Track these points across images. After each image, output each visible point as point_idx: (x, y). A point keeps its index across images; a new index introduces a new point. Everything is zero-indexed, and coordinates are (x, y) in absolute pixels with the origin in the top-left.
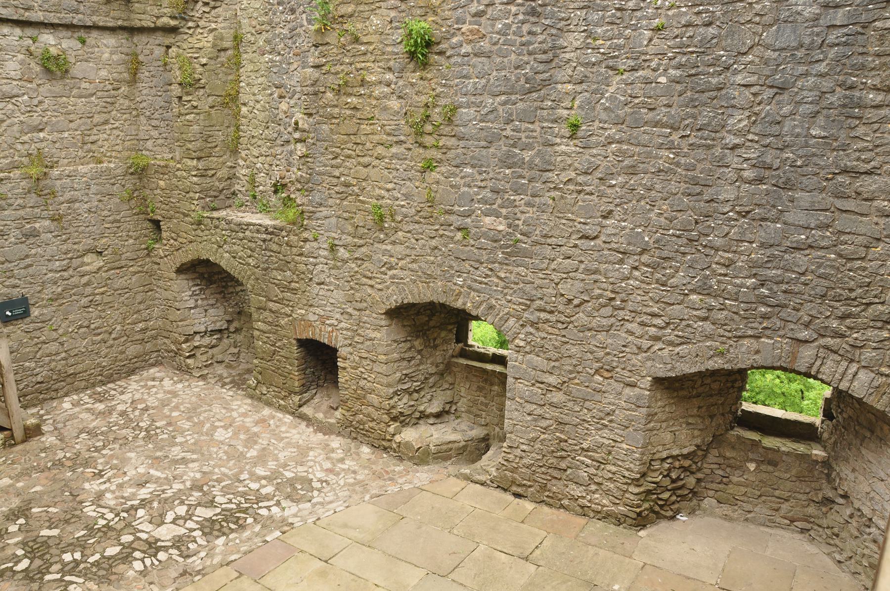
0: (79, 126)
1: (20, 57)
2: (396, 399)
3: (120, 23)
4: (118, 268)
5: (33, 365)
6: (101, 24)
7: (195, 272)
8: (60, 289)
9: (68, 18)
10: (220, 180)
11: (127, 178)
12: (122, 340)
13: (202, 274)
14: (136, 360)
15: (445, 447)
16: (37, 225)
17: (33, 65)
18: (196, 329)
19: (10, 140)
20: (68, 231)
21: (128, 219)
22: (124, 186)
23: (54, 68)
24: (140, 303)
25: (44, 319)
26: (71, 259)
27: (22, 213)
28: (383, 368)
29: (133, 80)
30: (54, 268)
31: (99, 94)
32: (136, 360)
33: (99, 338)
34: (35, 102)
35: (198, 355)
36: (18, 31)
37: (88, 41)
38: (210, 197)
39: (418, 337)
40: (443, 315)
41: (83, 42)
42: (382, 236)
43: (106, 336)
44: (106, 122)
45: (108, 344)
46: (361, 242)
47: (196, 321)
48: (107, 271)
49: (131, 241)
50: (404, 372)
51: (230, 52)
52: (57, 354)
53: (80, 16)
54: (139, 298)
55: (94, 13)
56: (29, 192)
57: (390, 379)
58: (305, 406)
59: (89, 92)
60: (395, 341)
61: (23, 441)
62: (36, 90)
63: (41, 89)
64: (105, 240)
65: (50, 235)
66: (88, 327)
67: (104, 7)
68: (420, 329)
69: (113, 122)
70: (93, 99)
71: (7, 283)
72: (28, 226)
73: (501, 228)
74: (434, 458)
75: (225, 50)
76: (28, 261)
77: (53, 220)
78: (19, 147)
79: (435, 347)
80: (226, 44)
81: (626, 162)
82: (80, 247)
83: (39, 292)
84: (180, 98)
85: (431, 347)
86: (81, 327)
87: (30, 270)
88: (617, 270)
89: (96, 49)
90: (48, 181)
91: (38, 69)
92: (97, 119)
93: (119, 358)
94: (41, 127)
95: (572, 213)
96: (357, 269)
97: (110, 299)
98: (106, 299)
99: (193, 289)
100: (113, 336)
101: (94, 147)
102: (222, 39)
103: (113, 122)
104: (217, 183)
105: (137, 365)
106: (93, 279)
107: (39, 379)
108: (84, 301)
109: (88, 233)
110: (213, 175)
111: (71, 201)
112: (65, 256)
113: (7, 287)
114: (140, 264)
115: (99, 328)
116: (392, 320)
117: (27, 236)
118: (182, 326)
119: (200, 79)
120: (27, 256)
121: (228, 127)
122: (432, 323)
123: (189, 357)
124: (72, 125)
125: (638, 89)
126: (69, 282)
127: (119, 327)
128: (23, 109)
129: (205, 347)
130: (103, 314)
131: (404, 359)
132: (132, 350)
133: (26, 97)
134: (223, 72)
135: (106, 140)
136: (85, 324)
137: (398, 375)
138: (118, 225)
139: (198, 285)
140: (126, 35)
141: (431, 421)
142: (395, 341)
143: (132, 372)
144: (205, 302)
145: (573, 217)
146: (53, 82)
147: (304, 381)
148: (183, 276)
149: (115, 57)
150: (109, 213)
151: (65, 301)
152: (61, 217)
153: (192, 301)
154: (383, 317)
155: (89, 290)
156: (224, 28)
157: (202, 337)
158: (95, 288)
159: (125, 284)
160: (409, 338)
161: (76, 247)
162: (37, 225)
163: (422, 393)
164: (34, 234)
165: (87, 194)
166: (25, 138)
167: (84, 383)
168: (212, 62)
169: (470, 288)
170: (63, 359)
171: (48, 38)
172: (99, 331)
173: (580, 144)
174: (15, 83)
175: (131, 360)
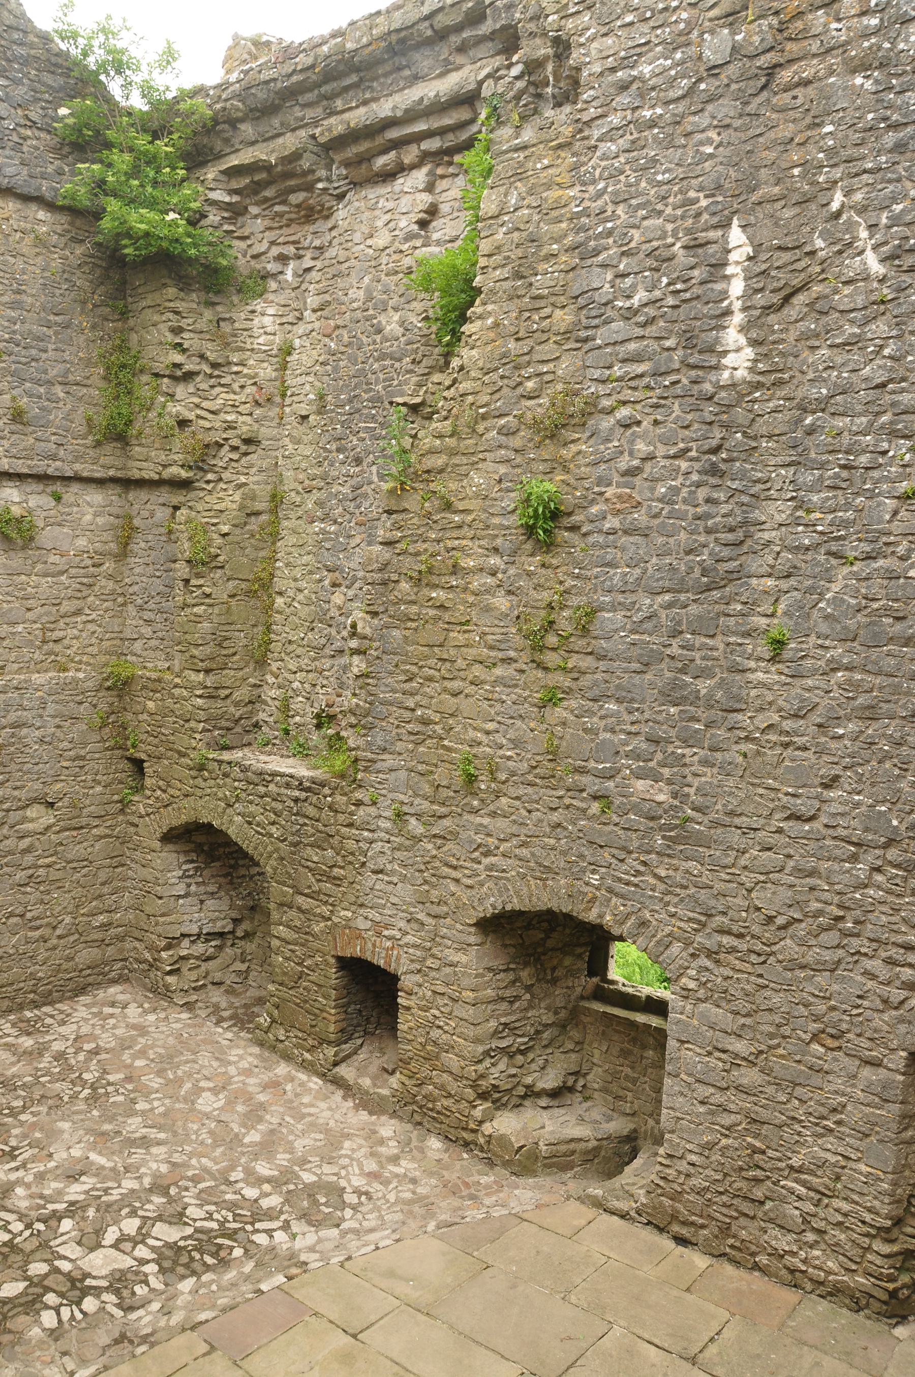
2: (487, 1062)
3: (111, 473)
4: (75, 829)
6: (85, 474)
10: (237, 704)
11: (100, 695)
12: (72, 938)
13: (200, 845)
15: (563, 1148)
18: (185, 930)
24: (103, 884)
26: (8, 811)
28: (468, 1012)
29: (123, 553)
31: (73, 571)
33: (37, 933)
35: (184, 970)
37: (65, 497)
38: (221, 729)
39: (526, 964)
41: (58, 499)
44: (78, 612)
45: (49, 945)
46: (443, 810)
49: (99, 789)
50: (503, 1020)
51: (264, 517)
53: (58, 463)
54: (103, 875)
55: (77, 459)
57: (479, 1030)
58: (344, 1065)
59: (58, 568)
60: (490, 969)
64: (59, 785)
66: (22, 916)
67: (91, 452)
68: (530, 951)
70: (63, 578)
74: (545, 1166)
75: (257, 514)
79: (554, 982)
81: (860, 700)
82: (22, 794)
84: (187, 581)
85: (548, 982)
86: (12, 915)
88: (848, 871)
89: (75, 509)
92: (66, 607)
93: (64, 967)
95: (775, 779)
96: (434, 852)
98: (54, 875)
99: (184, 867)
100: (58, 932)
101: (58, 648)
102: (253, 498)
104: (232, 709)
105: (90, 979)
106: (37, 843)
108: (21, 876)
109: (37, 773)
110: (227, 697)
115: (38, 918)
116: (487, 935)
119: (217, 556)
122: (550, 943)
123: (170, 973)
124: (29, 615)
125: (876, 587)
127: (68, 919)
129: (197, 958)
130: (47, 898)
132: (86, 955)
135: (76, 638)
137: (493, 1024)
138: (81, 763)
139: (192, 861)
140: (118, 490)
141: (544, 1102)
142: (490, 969)
145: (776, 785)
146: (11, 553)
147: (344, 1024)
148: (171, 847)
149: (100, 520)
154: (473, 930)
155: (29, 859)
157: (193, 942)
158: (39, 857)
159: (83, 854)
161: (16, 793)
163: (531, 1056)
165: (41, 716)
168: (238, 531)
169: (610, 890)
172: (38, 922)
173: (786, 671)
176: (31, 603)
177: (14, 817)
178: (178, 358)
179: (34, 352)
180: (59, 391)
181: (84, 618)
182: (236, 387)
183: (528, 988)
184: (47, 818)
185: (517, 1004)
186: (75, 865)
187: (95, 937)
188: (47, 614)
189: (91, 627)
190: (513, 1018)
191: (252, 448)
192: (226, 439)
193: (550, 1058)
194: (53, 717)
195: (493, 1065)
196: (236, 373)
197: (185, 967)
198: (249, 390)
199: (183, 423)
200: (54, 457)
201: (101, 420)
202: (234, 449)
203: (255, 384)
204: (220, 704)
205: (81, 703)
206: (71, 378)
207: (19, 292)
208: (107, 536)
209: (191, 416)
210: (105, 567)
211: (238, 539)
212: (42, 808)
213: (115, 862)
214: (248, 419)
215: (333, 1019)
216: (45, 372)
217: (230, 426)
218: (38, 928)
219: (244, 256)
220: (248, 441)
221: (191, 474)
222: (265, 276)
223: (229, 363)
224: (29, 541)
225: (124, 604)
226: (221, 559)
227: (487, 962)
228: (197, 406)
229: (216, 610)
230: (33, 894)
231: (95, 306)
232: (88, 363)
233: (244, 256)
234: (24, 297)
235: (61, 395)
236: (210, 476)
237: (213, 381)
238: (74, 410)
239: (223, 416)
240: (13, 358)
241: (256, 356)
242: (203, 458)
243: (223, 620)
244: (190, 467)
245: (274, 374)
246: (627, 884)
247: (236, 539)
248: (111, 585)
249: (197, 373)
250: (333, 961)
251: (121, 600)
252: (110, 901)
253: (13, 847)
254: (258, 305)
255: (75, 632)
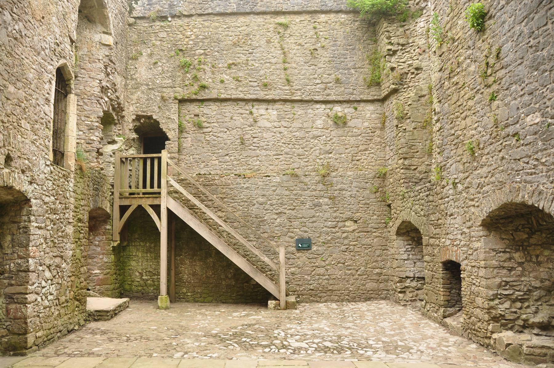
0: (351, 151)
1: (324, 118)
2: (497, 301)
3: (375, 97)
4: (365, 232)
5: (309, 278)
6: (365, 99)
7: (409, 236)
8: (330, 238)
9: (346, 98)
10: (420, 172)
11: (375, 180)
12: (364, 277)
13: (413, 238)
14: (372, 292)
15: (538, 351)
16: (321, 201)
17: (329, 121)
18: (408, 275)
19: (314, 157)
20: (337, 206)
21: (374, 203)
22: (373, 184)
23: (340, 122)
24: (378, 256)
25: (319, 253)
26: (338, 222)
27: (314, 193)
28: (482, 272)
29: (383, 128)
30: (328, 225)
31: (363, 135)
32: (372, 292)
33: (350, 272)
34: (329, 139)
35: (407, 292)
36: (323, 106)
37: (358, 108)
38: (412, 182)
39: (517, 250)
40: (544, 235)
41: (356, 109)
42: (475, 164)
43: (354, 272)
44: (366, 150)
45: (355, 277)
46: (467, 174)
47: (408, 269)
48: (359, 232)
49: (375, 217)
50: (504, 279)
51: (427, 97)
52: (323, 275)
53: (354, 96)
54: (378, 253)
55: (361, 94)
56: (319, 182)
57: (489, 282)
58: (448, 318)
59: (357, 134)
60: (494, 250)
61: (284, 309)
62: (330, 133)
63: (332, 133)
64: (359, 214)
65: (327, 207)
66: (344, 264)
67: (367, 91)
68: (519, 243)
69: (370, 149)
70: (359, 137)
71: (301, 229)
72: (316, 200)
73: (538, 120)
74: (526, 359)
75: (424, 96)
76: (314, 219)
77: (330, 199)
78: (318, 161)
79: (539, 263)
80: (424, 93)
82: (344, 216)
83: (318, 237)
84: (397, 126)
85: (534, 263)
86: (339, 263)
87: (315, 224)
89: (363, 112)
90: (329, 178)
91: (332, 123)
92: (361, 148)
93: (361, 288)
94: (330, 151)
96: (466, 196)
97: (359, 250)
98: (357, 249)
99: (407, 247)
100: (359, 273)
101: (358, 163)
102: (421, 90)
103: (370, 149)
104: (418, 175)
105: (373, 296)
106: (350, 236)
107: (311, 287)
108: (343, 248)
109: (350, 208)
110: (415, 169)
111: (341, 190)
112: (334, 220)
113: (302, 231)
114: (380, 232)
115: (350, 266)
116: (490, 232)
117: (315, 206)
118: (398, 271)
119: (407, 114)
120: (314, 216)
121: (426, 140)
122: (532, 241)
123: (400, 292)
124: (347, 151)
126: (335, 235)
127: (363, 268)
128: (322, 142)
129: (412, 288)
130: (353, 258)
131: (504, 267)
132: (370, 285)
133: (324, 137)
134: (423, 109)
135: (366, 159)
136: (341, 262)
137: (498, 280)
138: (368, 206)
139: (410, 245)
140: (380, 104)
141: (536, 331)
142: (494, 250)
143: (369, 299)
144: (415, 257)
146: (339, 129)
147: (449, 298)
148: (401, 238)
149: (373, 116)
150: (363, 199)
151: (331, 245)
152: (335, 197)
153: (406, 255)
154: (481, 228)
155: (346, 242)
156: (423, 84)
157: (412, 281)
158: (350, 241)
159: (369, 243)
160: (507, 250)
161: (341, 215)
162: (321, 201)
163: (526, 304)
164: (319, 205)
165: (351, 187)
166: (322, 157)
167: (337, 298)
168: (415, 103)
169: (526, 182)
170: (326, 279)
171: (338, 109)
172: (350, 267)
174: (320, 130)
175: (368, 291)
176: (347, 146)
177: (340, 224)
178: (390, 47)
179: (342, 59)
180: (353, 71)
181: (369, 152)
182: (412, 51)
183: (520, 264)
184: (355, 226)
185: (513, 272)
186: (366, 246)
187: (375, 278)
188: (354, 150)
189: (372, 155)
190: (512, 279)
191: (419, 72)
192: (409, 71)
193: (540, 307)
194: (355, 187)
195: (500, 303)
196: (412, 46)
197: (408, 291)
198: (417, 50)
199: (393, 69)
200: (352, 94)
201: (368, 80)
202: (413, 73)
203: (418, 48)
204: (411, 172)
205: (367, 183)
206: (357, 66)
207: (335, 41)
208: (377, 121)
209: (396, 66)
210: (376, 133)
211: (416, 106)
212: (352, 223)
213: (383, 248)
214: (417, 61)
215: (442, 293)
216: (347, 65)
217: (410, 65)
218: (350, 270)
219: (413, 5)
220: (417, 69)
221: (397, 86)
222: (422, 9)
223: (409, 43)
224: (345, 123)
225: (385, 147)
226: (408, 115)
227: (491, 246)
228: (398, 62)
229: (407, 134)
230: (348, 256)
231: (364, 41)
232: (363, 60)
233: (413, 5)
234: (337, 42)
235: (354, 72)
236: (405, 86)
237: (402, 52)
238: (359, 77)
239: (407, 63)
240: (335, 62)
241: (418, 38)
242: (402, 79)
243: (411, 138)
244: (397, 84)
245: (425, 41)
246: (531, 175)
247: (414, 106)
248: (379, 139)
249: (398, 51)
250: (440, 265)
251: (383, 145)
252: (381, 264)
253: (340, 236)
254: (419, 20)
255: (365, 157)
